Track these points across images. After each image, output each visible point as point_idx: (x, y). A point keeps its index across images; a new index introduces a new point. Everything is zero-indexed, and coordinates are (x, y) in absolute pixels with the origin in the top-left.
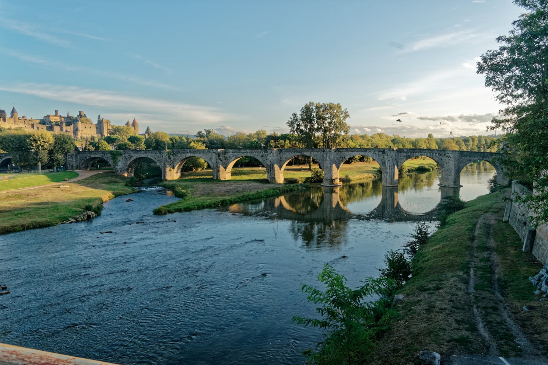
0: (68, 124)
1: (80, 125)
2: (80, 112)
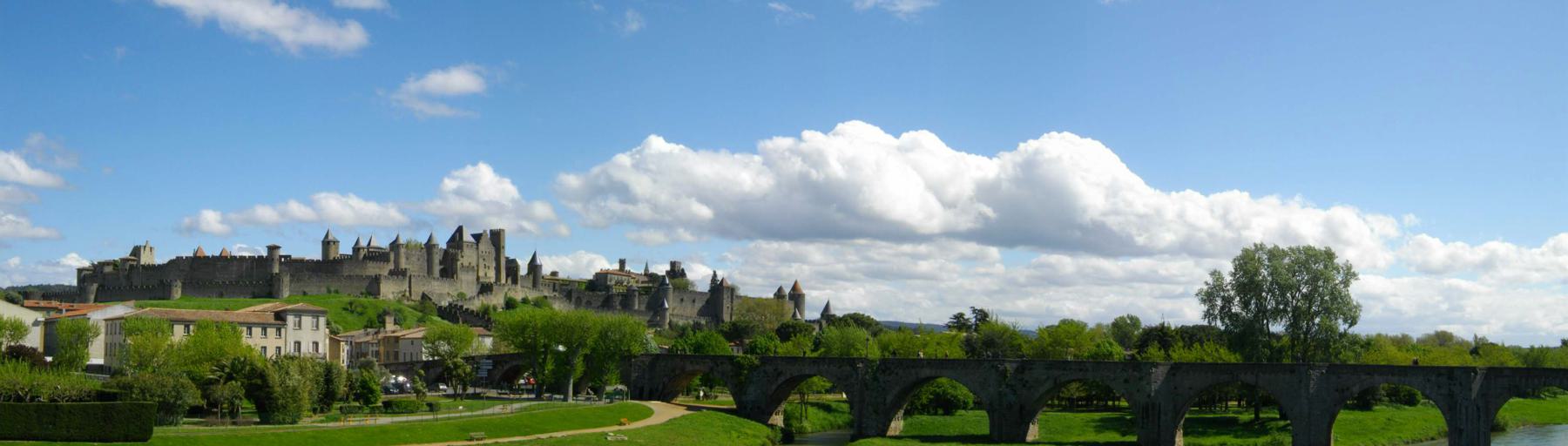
2: (673, 264)
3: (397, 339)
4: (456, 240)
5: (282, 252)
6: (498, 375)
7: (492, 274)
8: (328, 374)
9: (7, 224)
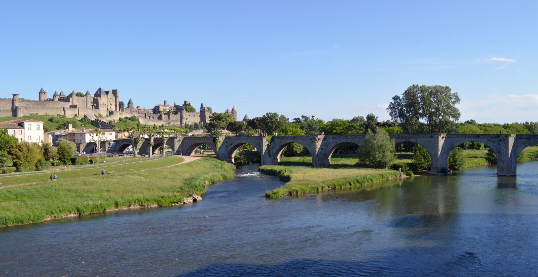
0: (175, 113)
1: (185, 114)
2: (185, 102)
3: (74, 134)
4: (98, 94)
5: (20, 97)
6: (118, 148)
7: (113, 108)
8: (46, 150)
9: (537, 181)
